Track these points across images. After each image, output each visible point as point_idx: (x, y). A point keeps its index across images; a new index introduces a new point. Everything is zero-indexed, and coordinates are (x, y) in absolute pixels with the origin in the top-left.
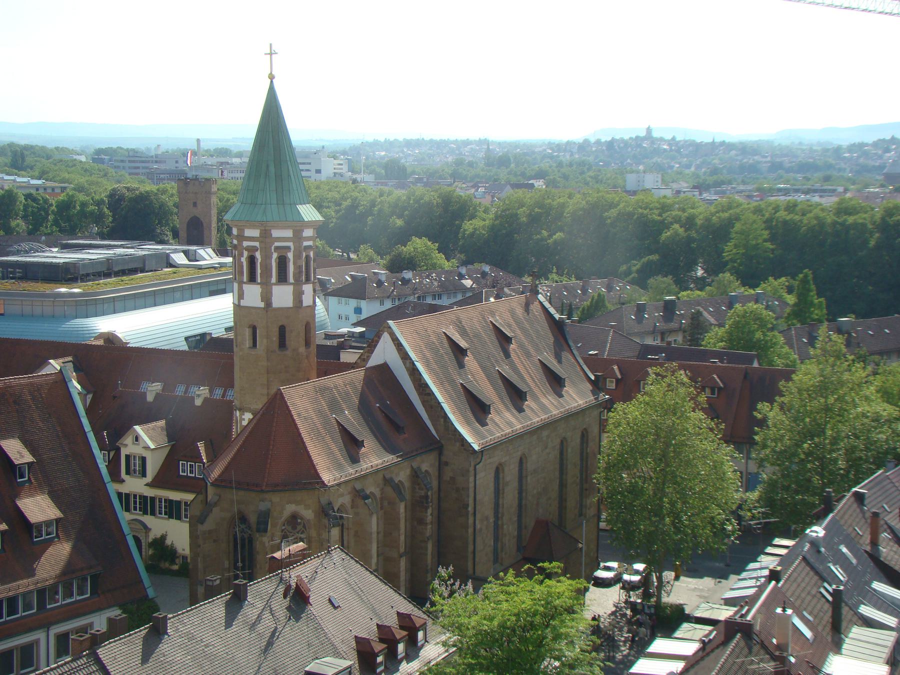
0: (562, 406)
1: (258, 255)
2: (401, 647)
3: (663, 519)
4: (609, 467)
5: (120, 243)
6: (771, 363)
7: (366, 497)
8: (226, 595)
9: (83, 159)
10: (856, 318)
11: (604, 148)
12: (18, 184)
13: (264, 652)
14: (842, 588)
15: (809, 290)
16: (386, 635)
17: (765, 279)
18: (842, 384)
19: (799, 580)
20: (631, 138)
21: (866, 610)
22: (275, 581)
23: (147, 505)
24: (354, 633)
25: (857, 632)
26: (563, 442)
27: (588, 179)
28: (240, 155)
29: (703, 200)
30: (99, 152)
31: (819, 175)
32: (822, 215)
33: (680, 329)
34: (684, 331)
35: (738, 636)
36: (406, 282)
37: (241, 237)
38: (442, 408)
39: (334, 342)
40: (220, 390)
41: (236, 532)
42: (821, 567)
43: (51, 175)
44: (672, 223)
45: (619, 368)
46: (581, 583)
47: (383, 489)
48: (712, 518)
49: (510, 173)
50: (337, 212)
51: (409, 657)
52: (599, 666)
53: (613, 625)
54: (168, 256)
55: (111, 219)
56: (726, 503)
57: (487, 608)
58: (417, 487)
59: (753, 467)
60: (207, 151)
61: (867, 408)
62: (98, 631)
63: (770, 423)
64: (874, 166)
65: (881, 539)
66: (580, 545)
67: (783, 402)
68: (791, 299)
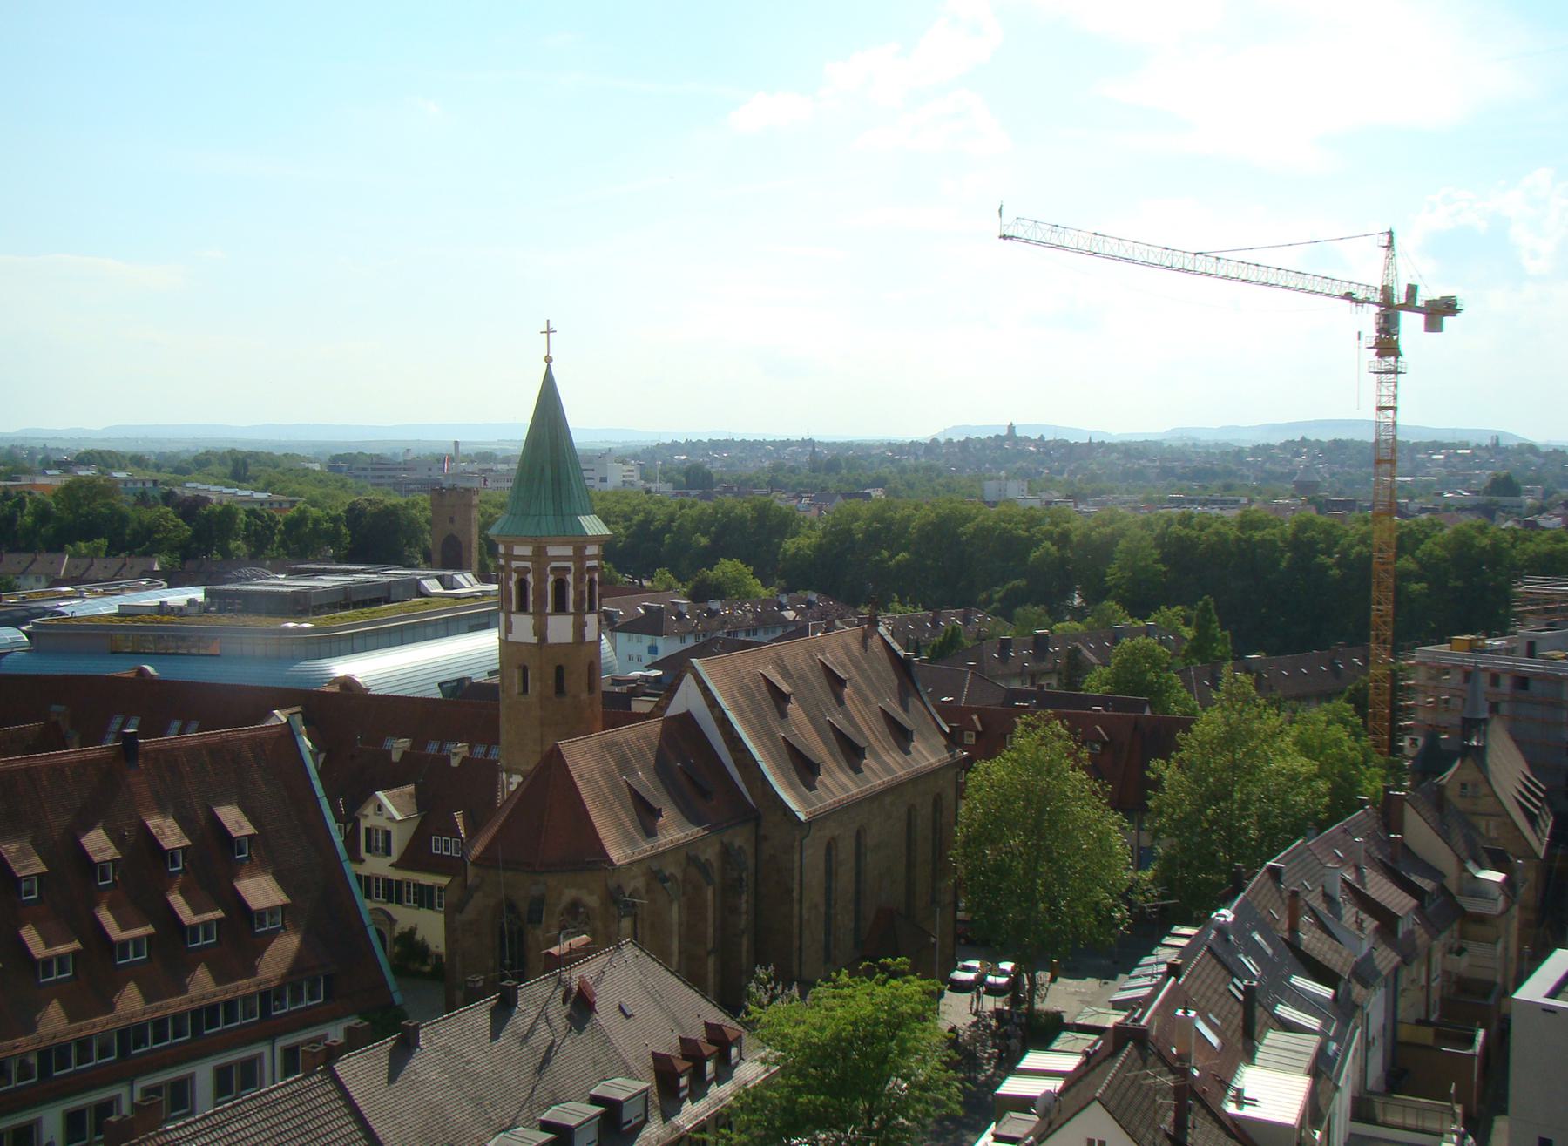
0: (910, 765)
1: (530, 578)
2: (710, 1066)
3: (1035, 904)
4: (968, 841)
5: (360, 568)
6: (1166, 710)
7: (665, 879)
8: (491, 1000)
9: (317, 467)
10: (1267, 655)
11: (957, 450)
12: (239, 498)
13: (539, 1071)
14: (1255, 983)
15: (1211, 621)
16: (689, 1048)
17: (1156, 608)
18: (1252, 734)
19: (1204, 975)
20: (989, 438)
21: (1285, 1011)
22: (552, 983)
23: (393, 891)
24: (651, 1049)
25: (1272, 1037)
26: (911, 810)
27: (938, 488)
28: (506, 460)
29: (1081, 512)
30: (336, 458)
31: (1218, 483)
32: (1223, 529)
33: (1054, 670)
34: (1060, 673)
35: (1130, 1045)
36: (713, 614)
37: (510, 556)
38: (759, 767)
39: (624, 689)
41: (503, 924)
42: (1230, 959)
43: (277, 488)
44: (1041, 541)
45: (980, 718)
46: (932, 984)
48: (1097, 903)
49: (840, 481)
50: (627, 528)
51: (721, 1079)
52: (957, 1087)
53: (974, 1039)
54: (418, 583)
55: (349, 539)
56: (1114, 885)
57: (814, 1017)
59: (1146, 840)
60: (468, 456)
61: (1283, 764)
62: (334, 1041)
63: (1166, 785)
64: (1282, 473)
65: (1301, 923)
66: (933, 940)
67: (1181, 759)
68: (1188, 633)
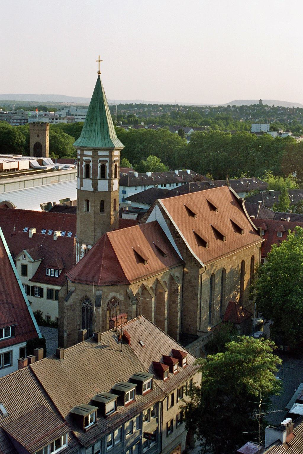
1: (91, 164)
20: (251, 105)
37: (82, 155)
38: (185, 244)
40: (64, 232)
47: (157, 285)
58: (173, 284)
